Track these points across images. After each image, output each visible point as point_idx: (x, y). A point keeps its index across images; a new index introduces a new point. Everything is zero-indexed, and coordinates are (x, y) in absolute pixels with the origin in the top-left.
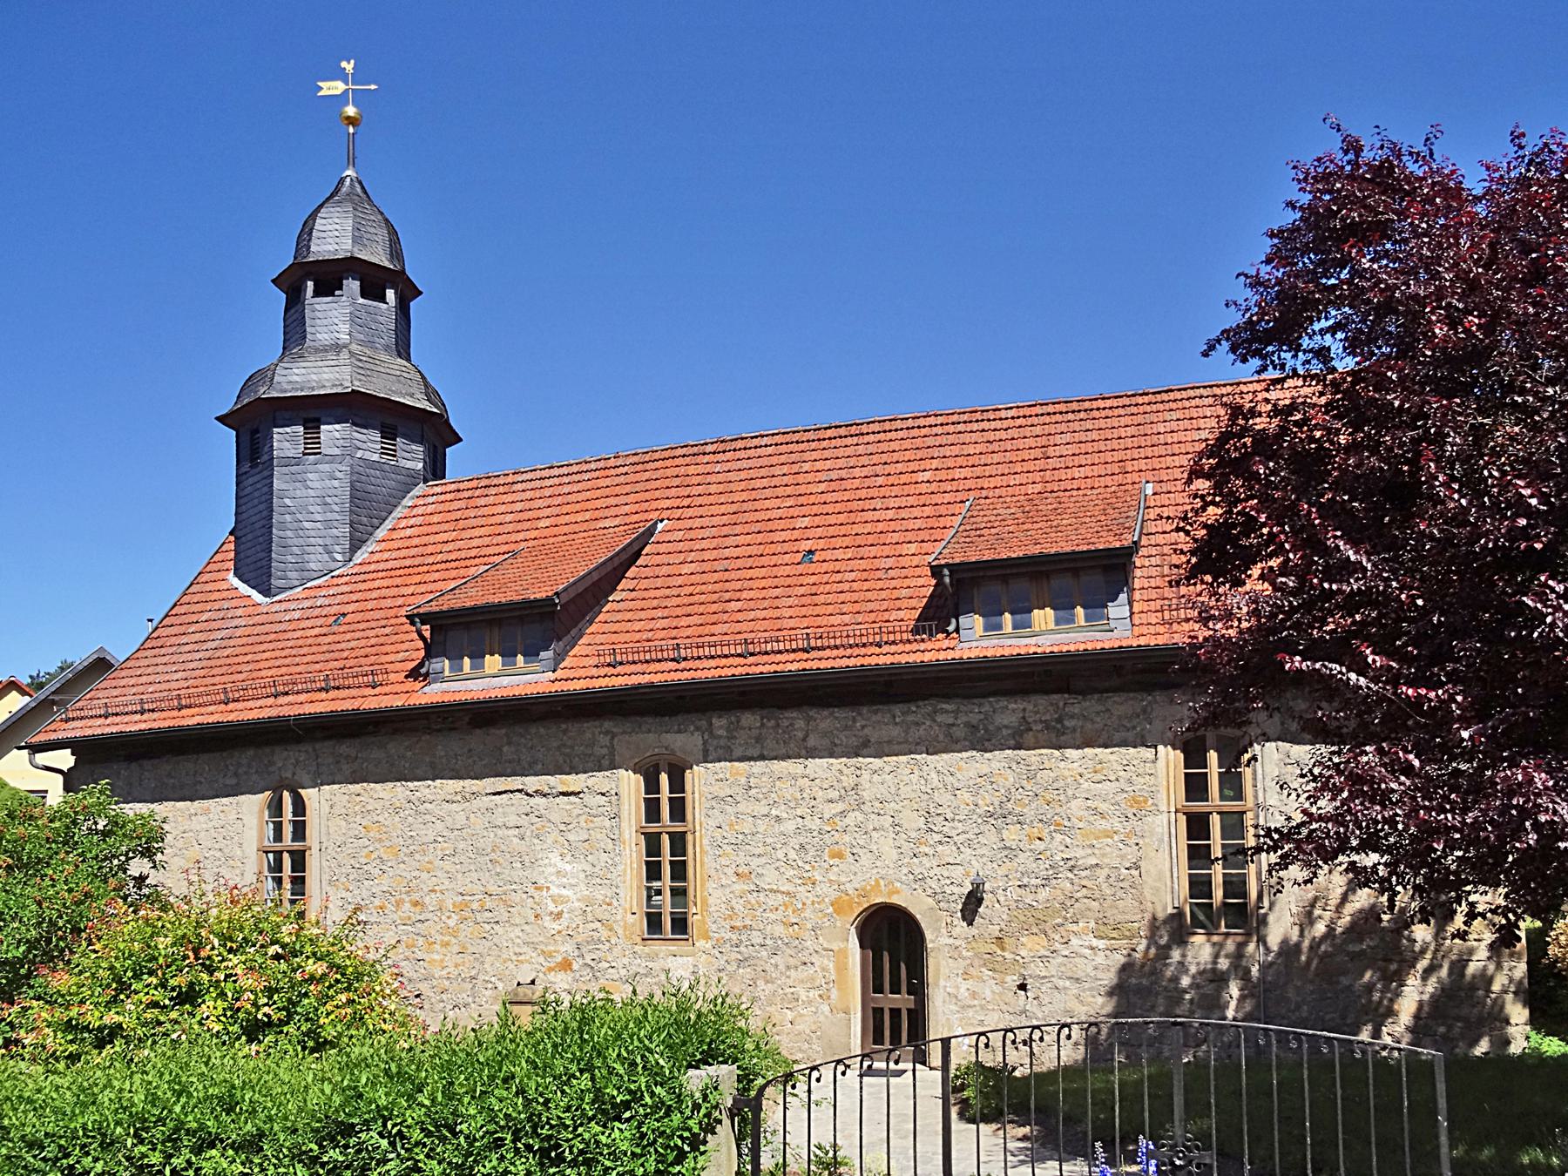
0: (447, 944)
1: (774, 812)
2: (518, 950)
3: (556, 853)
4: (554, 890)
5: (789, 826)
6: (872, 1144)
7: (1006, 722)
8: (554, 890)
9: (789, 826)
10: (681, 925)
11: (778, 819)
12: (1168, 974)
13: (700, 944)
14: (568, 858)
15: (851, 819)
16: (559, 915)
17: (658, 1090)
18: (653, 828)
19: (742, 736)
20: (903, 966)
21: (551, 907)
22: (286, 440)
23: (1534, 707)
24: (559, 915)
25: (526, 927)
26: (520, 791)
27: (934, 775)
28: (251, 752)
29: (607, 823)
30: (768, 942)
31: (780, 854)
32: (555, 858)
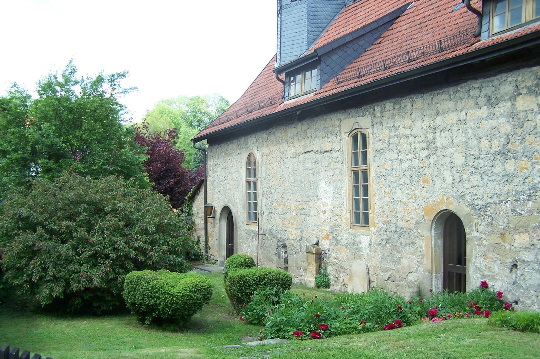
1: (400, 157)
5: (406, 165)
6: (201, 230)
7: (506, 91)
9: (406, 165)
10: (367, 221)
11: (401, 161)
12: (447, 290)
13: (372, 229)
15: (432, 159)
17: (196, 295)
18: (356, 168)
19: (387, 114)
27: (469, 130)
28: (243, 139)
29: (340, 166)
30: (398, 230)
31: (402, 180)
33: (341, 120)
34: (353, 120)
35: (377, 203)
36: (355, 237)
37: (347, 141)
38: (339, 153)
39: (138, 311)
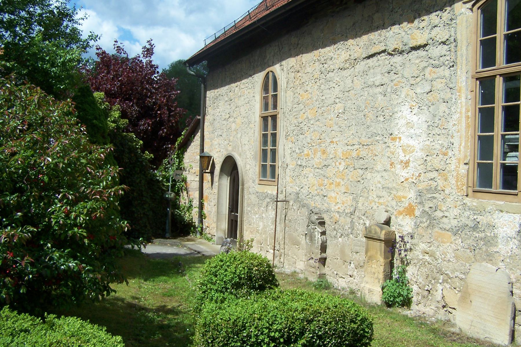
0: (339, 184)
2: (380, 194)
3: (407, 106)
4: (405, 141)
8: (405, 141)
10: (510, 175)
14: (415, 111)
16: (406, 164)
20: (150, 249)
21: (402, 157)
22: (278, 200)
23: (72, 300)
24: (406, 164)
25: (385, 174)
26: (384, 51)
29: (447, 73)
32: (405, 110)
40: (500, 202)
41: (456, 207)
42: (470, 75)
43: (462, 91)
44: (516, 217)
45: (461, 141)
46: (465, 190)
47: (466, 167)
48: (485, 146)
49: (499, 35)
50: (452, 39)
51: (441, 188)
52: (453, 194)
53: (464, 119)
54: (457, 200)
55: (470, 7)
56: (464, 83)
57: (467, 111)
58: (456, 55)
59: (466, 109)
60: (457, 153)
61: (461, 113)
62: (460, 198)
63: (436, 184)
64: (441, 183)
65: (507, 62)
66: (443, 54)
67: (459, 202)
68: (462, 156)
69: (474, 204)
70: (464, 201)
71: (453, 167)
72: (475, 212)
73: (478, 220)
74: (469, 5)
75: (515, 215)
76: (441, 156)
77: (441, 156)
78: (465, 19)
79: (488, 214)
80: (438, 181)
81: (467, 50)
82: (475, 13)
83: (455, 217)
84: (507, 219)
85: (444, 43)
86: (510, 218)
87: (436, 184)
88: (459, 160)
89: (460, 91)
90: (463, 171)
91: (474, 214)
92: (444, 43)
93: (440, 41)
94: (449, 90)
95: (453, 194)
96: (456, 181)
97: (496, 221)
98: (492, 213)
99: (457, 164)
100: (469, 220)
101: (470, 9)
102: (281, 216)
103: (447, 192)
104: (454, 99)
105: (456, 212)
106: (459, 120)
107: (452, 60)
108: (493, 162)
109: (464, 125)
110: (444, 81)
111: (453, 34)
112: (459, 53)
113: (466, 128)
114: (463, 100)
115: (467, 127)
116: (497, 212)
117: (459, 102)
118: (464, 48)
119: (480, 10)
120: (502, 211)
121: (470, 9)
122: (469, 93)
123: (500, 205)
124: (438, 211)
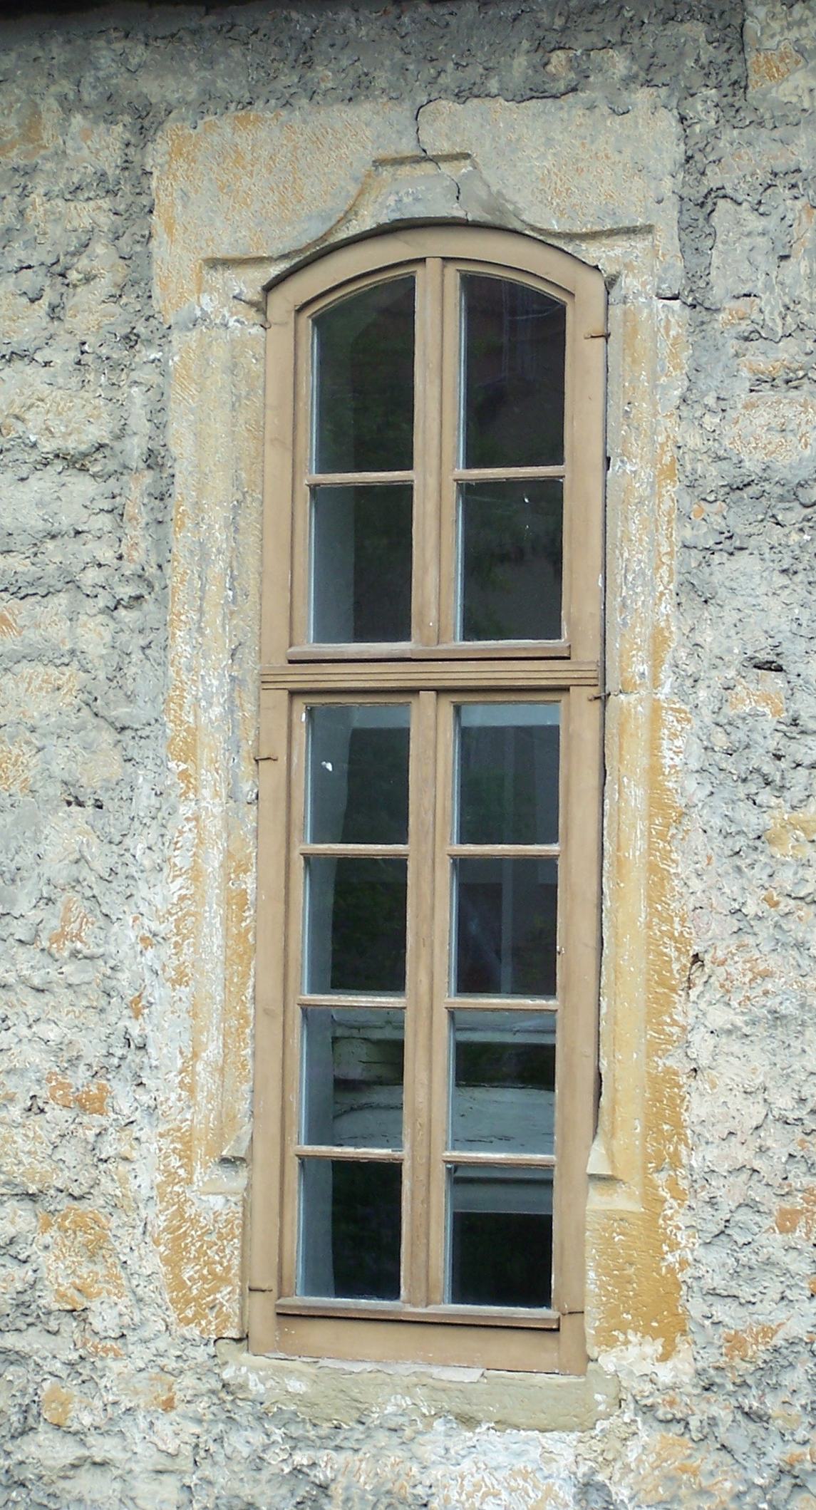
29: (93, 635)
33: (146, 122)
34: (366, 128)
35: (730, 1072)
36: (333, 1439)
37: (231, 408)
38: (82, 487)
39: (178, 1238)
40: (462, 1370)
41: (169, 1405)
42: (250, 665)
43: (205, 755)
44: (558, 1448)
45: (196, 1032)
46: (231, 1308)
47: (237, 1181)
48: (357, 1076)
49: (432, 482)
50: (135, 448)
51: (62, 1296)
52: (147, 1333)
53: (214, 913)
54: (172, 1364)
55: (253, 294)
56: (216, 711)
57: (234, 865)
58: (162, 545)
59: (229, 855)
60: (172, 1098)
61: (196, 874)
62: (201, 1354)
63: (27, 1273)
64: (58, 1271)
65: (472, 630)
66: (65, 522)
67: (188, 1380)
68: (202, 1116)
69: (296, 1386)
70: (227, 1374)
71: (145, 1179)
72: (295, 1431)
73: (320, 1475)
74: (250, 282)
75: (548, 1439)
76: (55, 1113)
77: (55, 1113)
78: (220, 353)
79: (382, 1438)
80: (45, 1260)
81: (233, 526)
82: (281, 338)
83: (164, 1463)
84: (502, 1459)
85: (76, 462)
86: (519, 1455)
87: (27, 1273)
88: (186, 1144)
89: (188, 752)
90: (217, 1202)
91: (295, 1443)
92: (76, 462)
93: (48, 446)
94: (108, 736)
95: (147, 1333)
96: (166, 1261)
97: (436, 1473)
98: (408, 1432)
99: (175, 1162)
100: (265, 1475)
101: (251, 304)
102: (445, 787)
103: (105, 1318)
104: (146, 789)
105: (173, 1433)
106: (185, 917)
107: (128, 569)
108: (405, 1154)
109: (214, 941)
110: (71, 677)
111: (139, 422)
112: (181, 541)
113: (228, 962)
114: (212, 803)
115: (240, 952)
116: (438, 1425)
117: (185, 810)
118: (217, 515)
119: (306, 322)
120: (469, 1421)
121: (251, 304)
122: (246, 767)
123: (463, 1391)
124: (44, 1436)
